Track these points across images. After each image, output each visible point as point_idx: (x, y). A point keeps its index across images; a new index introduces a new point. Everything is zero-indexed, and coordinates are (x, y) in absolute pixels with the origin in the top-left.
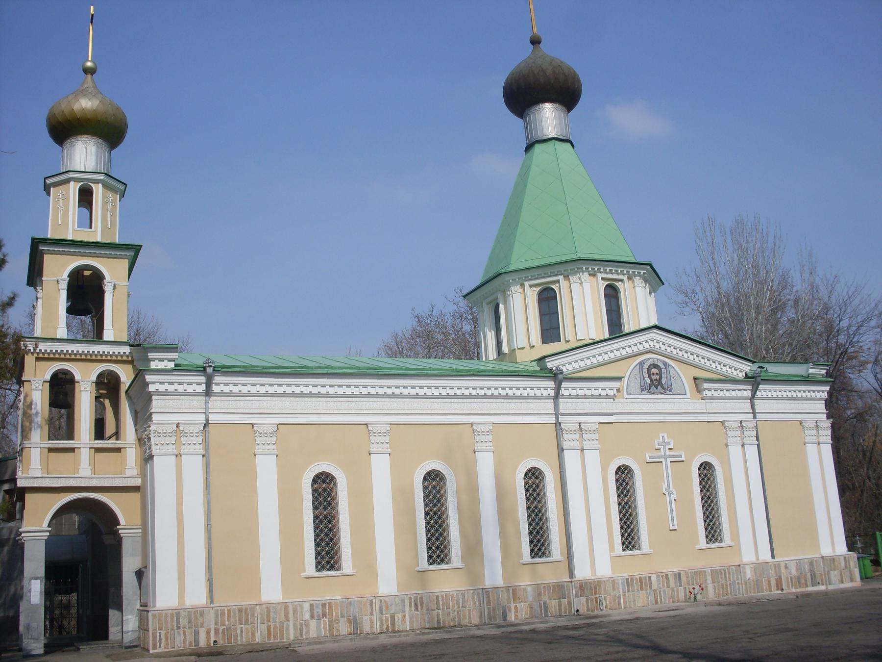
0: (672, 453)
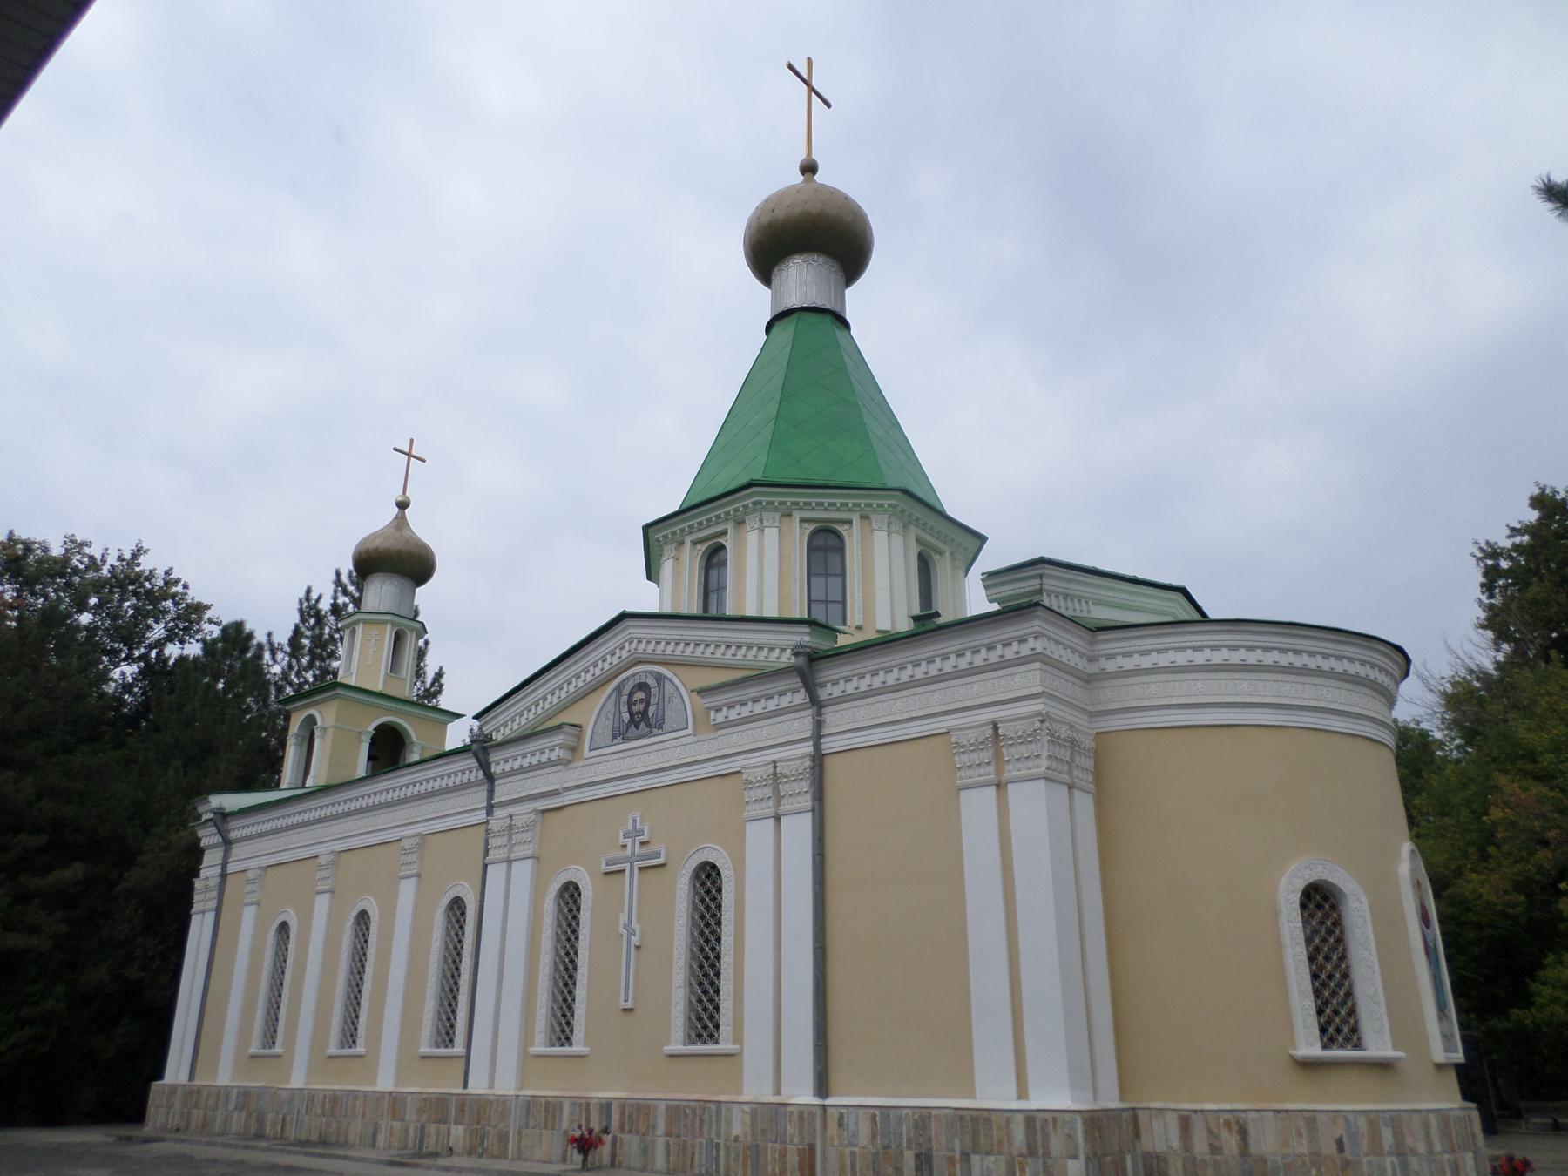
0: (646, 850)
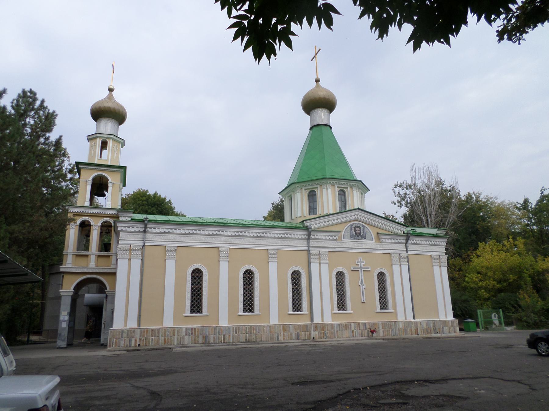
0: (364, 267)
